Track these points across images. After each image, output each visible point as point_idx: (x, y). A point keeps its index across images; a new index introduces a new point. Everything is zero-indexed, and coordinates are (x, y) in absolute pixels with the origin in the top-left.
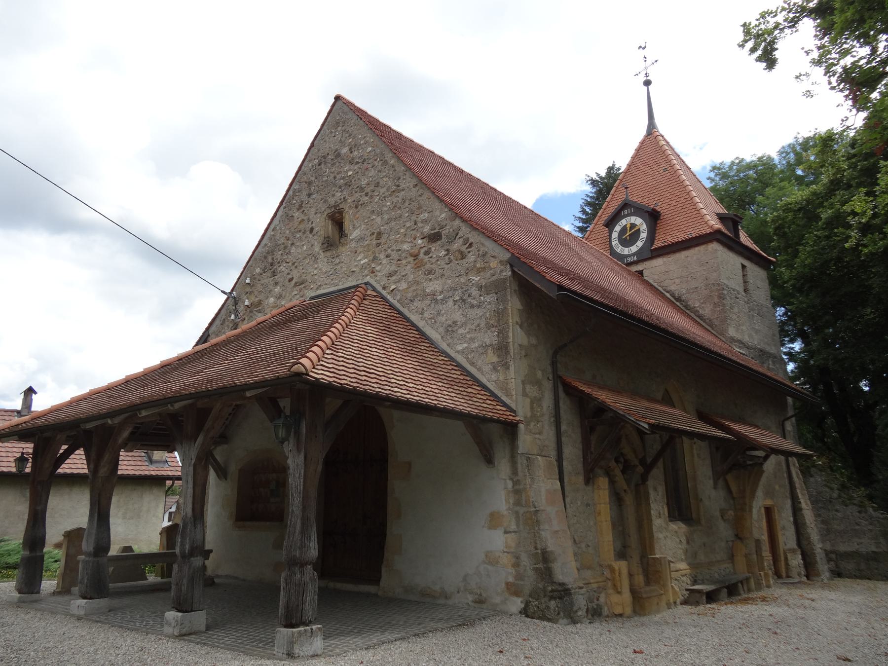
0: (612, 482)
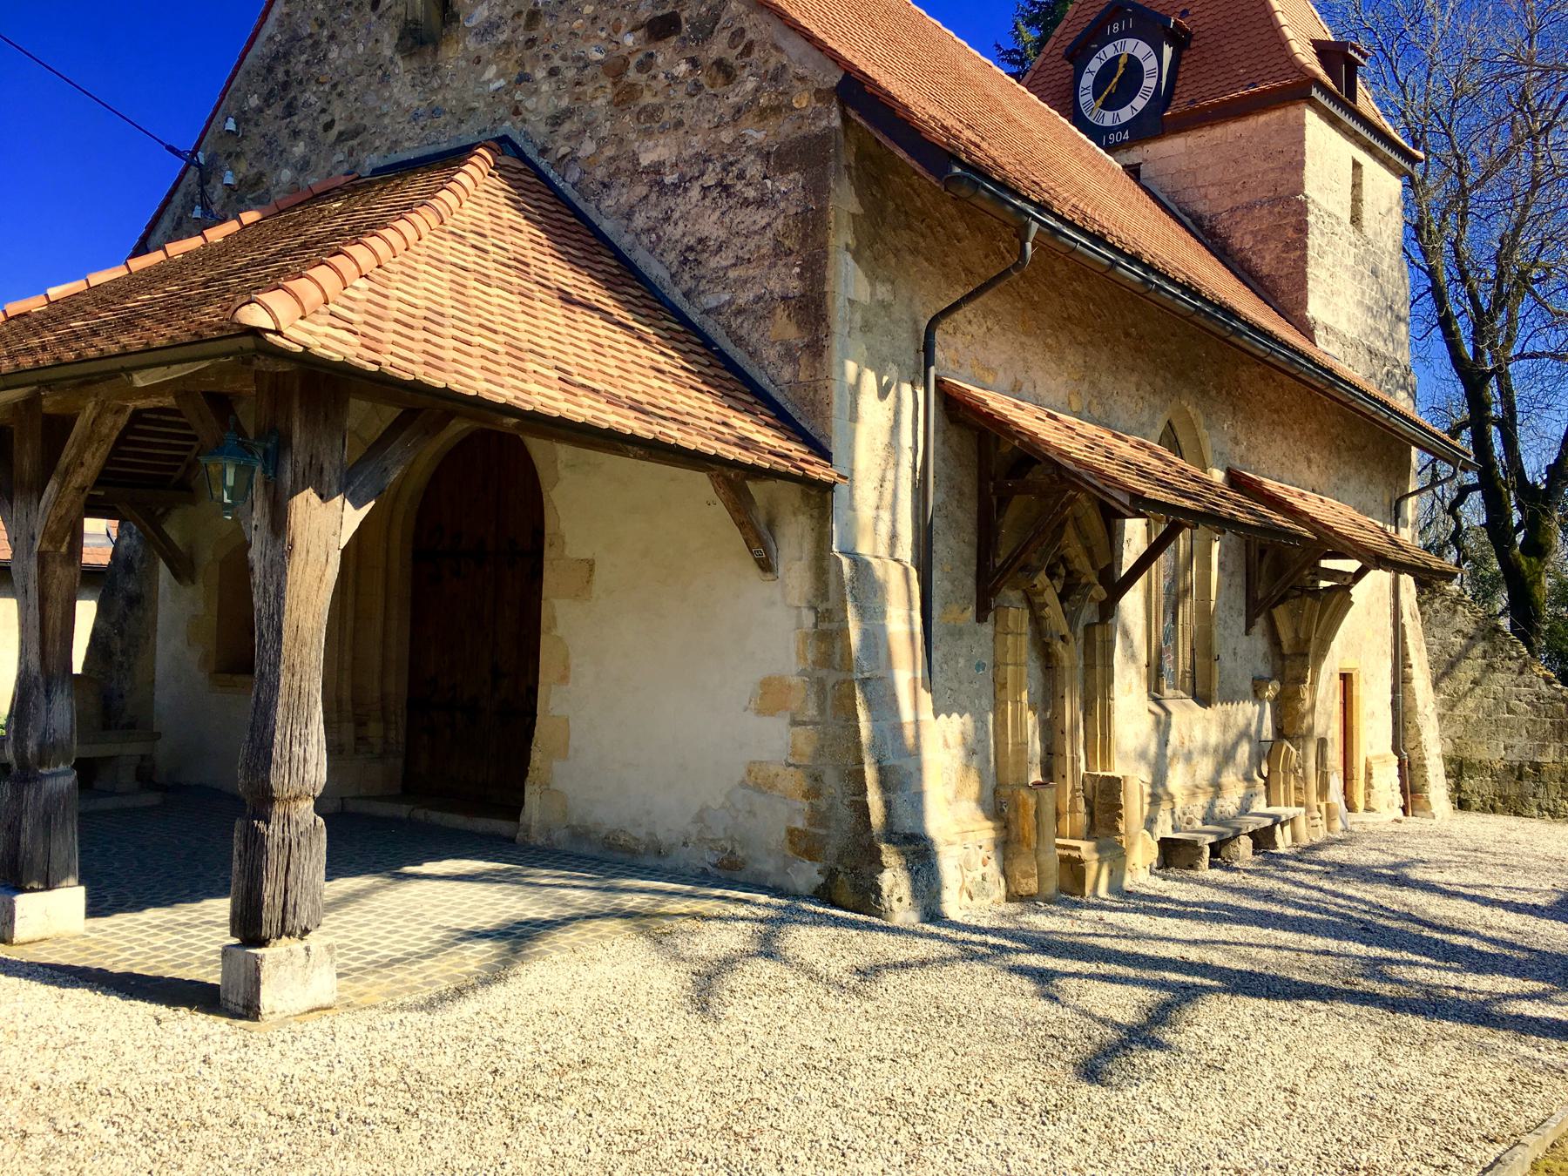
0: (1037, 621)
